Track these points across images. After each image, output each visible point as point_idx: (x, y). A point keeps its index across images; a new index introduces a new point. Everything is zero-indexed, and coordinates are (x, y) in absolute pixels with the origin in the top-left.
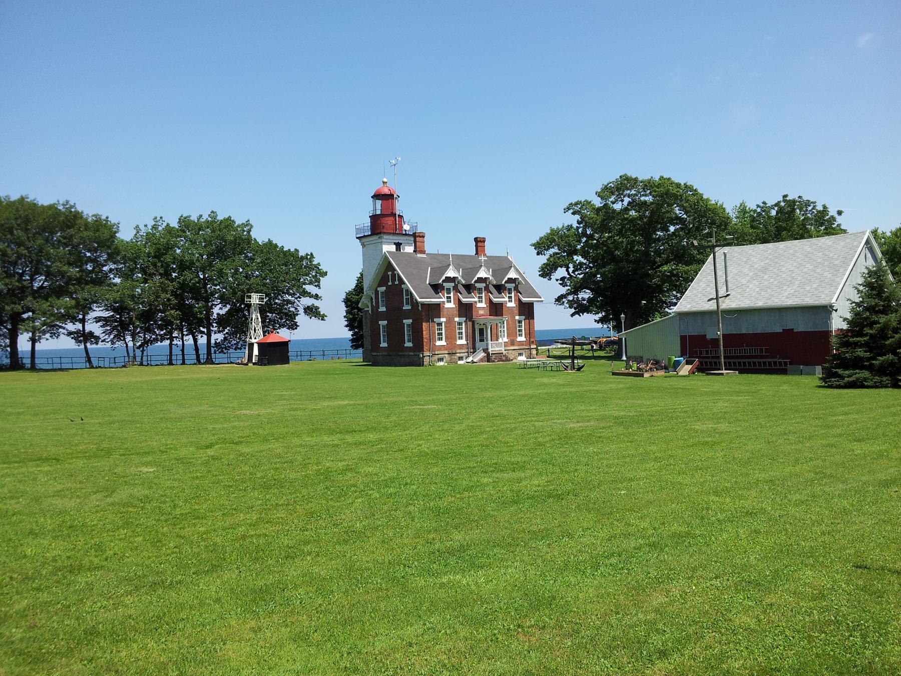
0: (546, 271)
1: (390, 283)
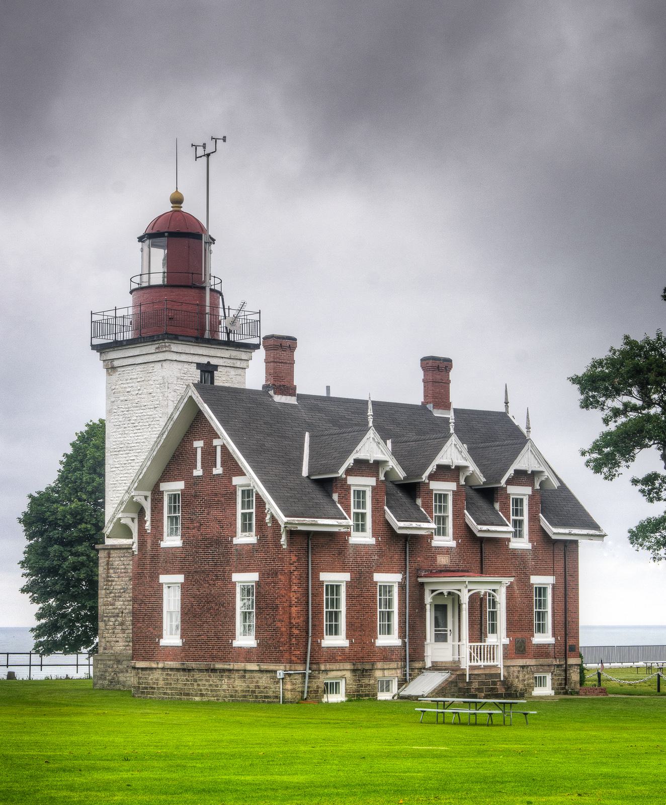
0: (610, 453)
1: (198, 472)
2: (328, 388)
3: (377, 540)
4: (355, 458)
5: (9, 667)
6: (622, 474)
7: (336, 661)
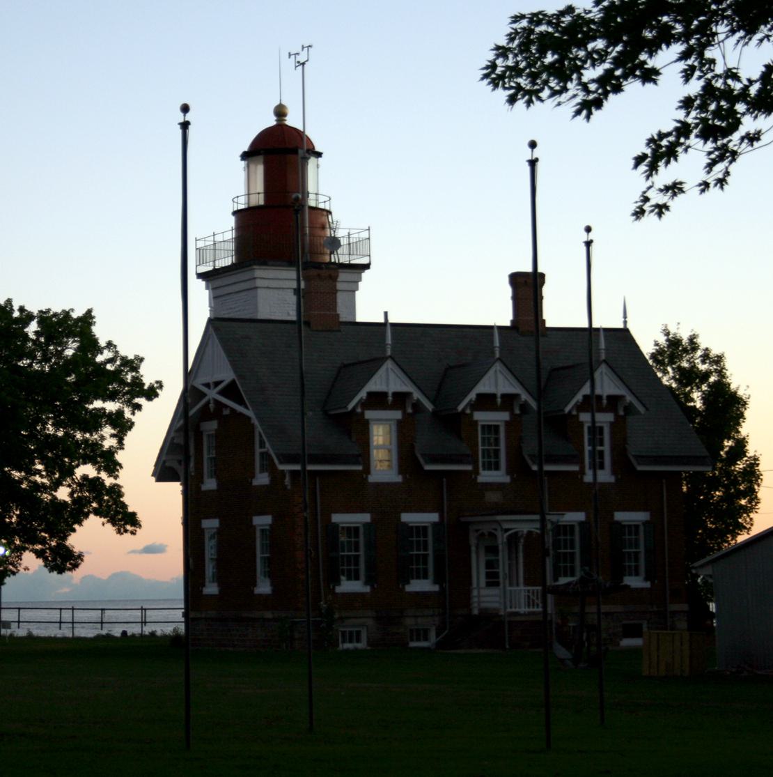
2: (386, 314)
3: (404, 478)
5: (147, 624)
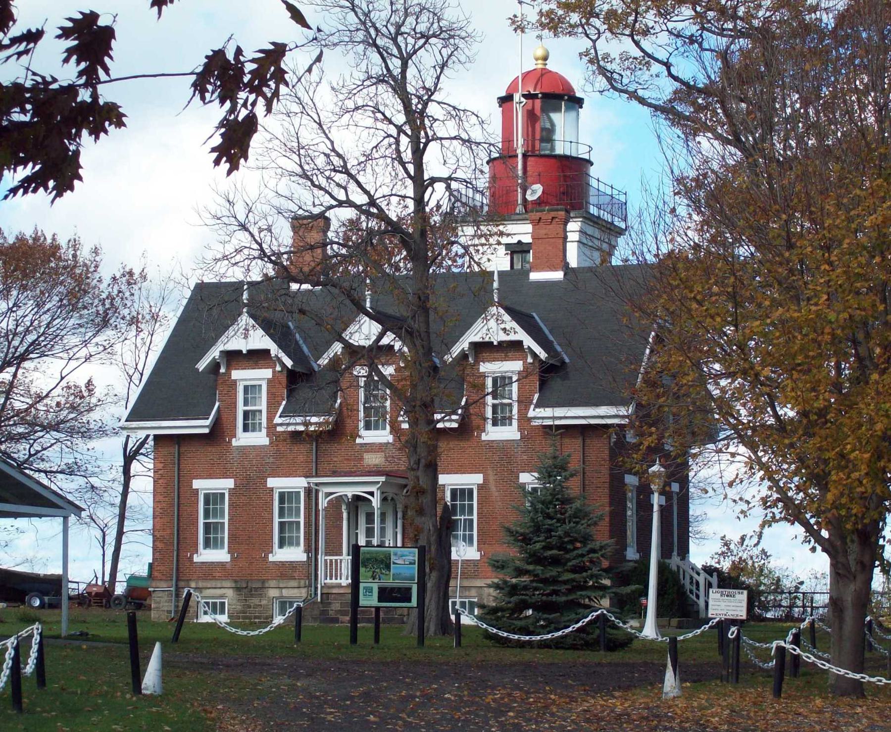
4: (12, 37)
6: (54, 235)
7: (214, 578)
